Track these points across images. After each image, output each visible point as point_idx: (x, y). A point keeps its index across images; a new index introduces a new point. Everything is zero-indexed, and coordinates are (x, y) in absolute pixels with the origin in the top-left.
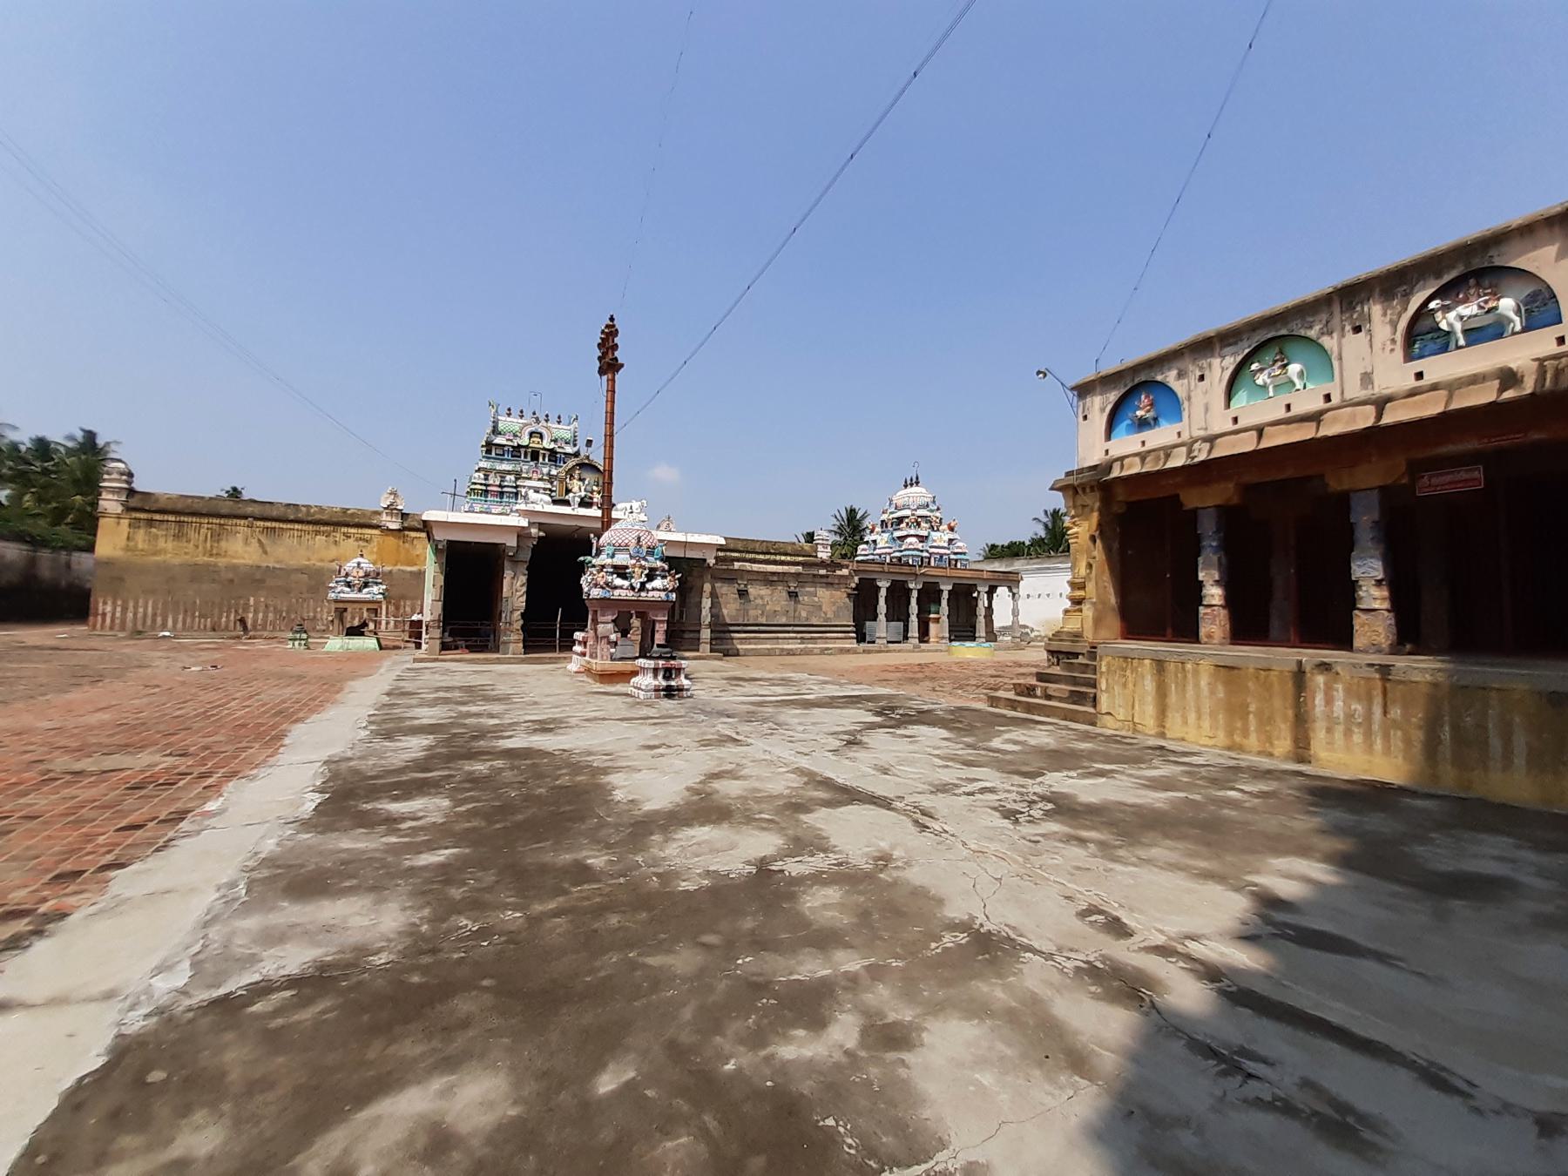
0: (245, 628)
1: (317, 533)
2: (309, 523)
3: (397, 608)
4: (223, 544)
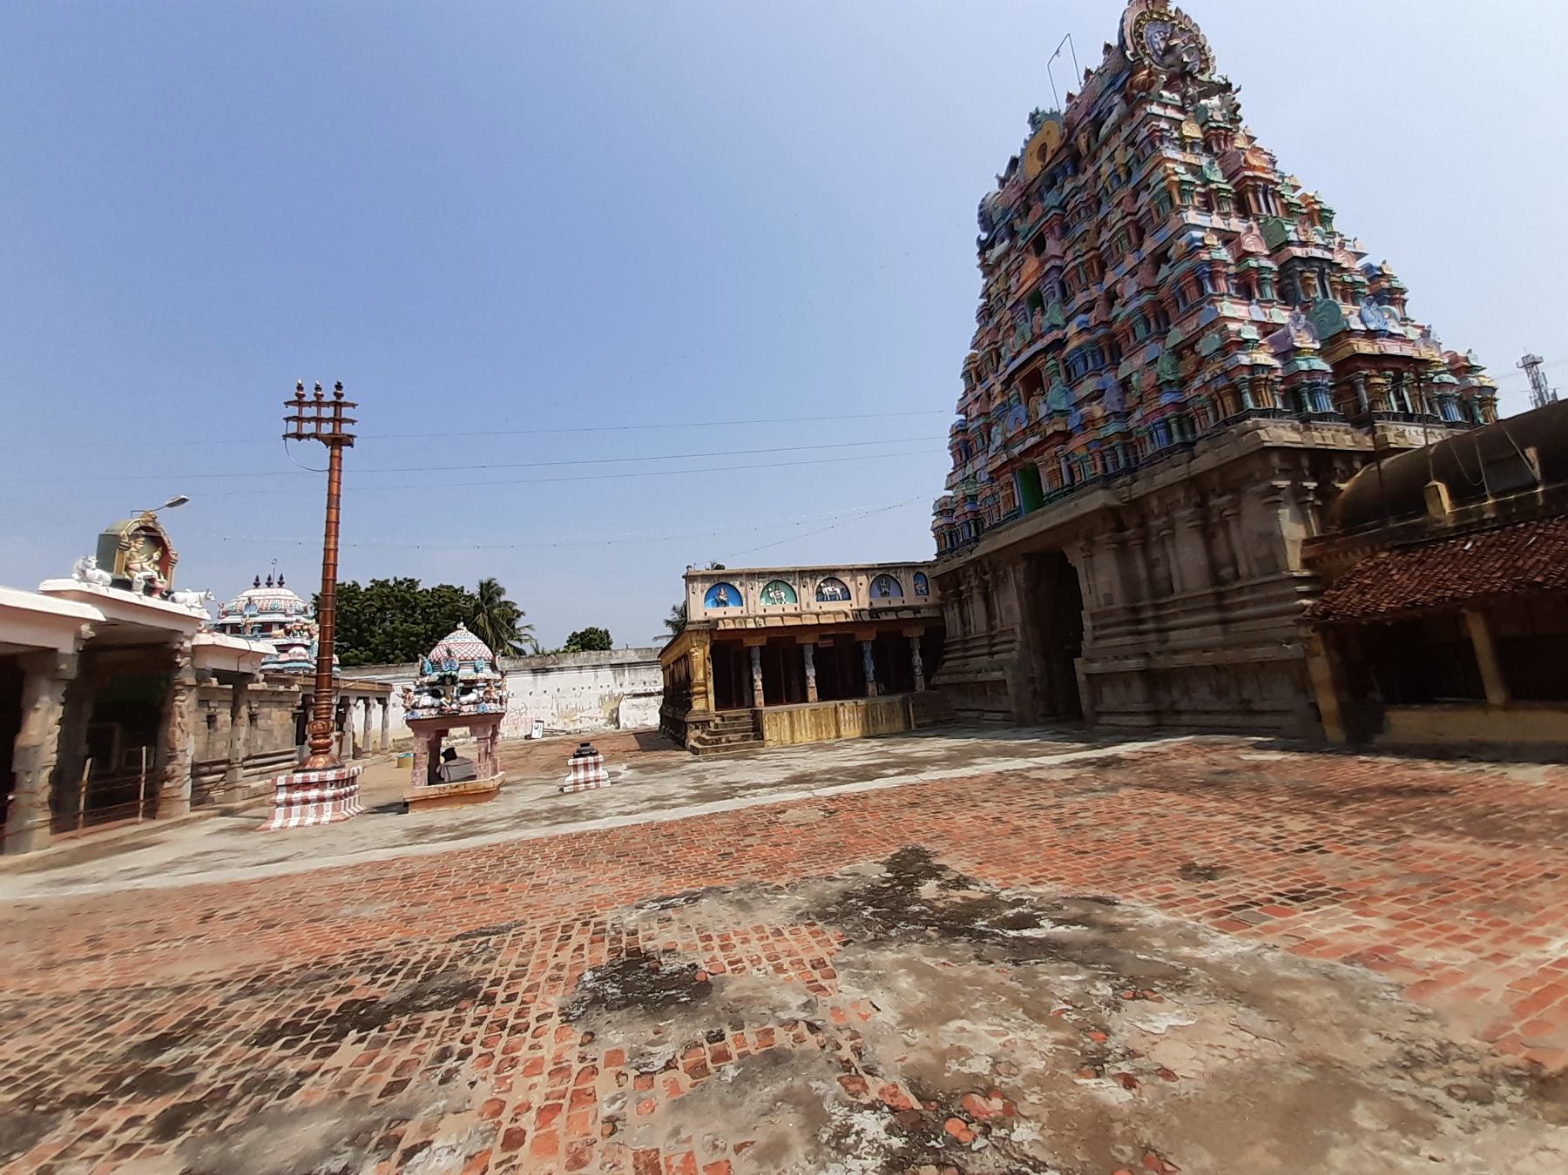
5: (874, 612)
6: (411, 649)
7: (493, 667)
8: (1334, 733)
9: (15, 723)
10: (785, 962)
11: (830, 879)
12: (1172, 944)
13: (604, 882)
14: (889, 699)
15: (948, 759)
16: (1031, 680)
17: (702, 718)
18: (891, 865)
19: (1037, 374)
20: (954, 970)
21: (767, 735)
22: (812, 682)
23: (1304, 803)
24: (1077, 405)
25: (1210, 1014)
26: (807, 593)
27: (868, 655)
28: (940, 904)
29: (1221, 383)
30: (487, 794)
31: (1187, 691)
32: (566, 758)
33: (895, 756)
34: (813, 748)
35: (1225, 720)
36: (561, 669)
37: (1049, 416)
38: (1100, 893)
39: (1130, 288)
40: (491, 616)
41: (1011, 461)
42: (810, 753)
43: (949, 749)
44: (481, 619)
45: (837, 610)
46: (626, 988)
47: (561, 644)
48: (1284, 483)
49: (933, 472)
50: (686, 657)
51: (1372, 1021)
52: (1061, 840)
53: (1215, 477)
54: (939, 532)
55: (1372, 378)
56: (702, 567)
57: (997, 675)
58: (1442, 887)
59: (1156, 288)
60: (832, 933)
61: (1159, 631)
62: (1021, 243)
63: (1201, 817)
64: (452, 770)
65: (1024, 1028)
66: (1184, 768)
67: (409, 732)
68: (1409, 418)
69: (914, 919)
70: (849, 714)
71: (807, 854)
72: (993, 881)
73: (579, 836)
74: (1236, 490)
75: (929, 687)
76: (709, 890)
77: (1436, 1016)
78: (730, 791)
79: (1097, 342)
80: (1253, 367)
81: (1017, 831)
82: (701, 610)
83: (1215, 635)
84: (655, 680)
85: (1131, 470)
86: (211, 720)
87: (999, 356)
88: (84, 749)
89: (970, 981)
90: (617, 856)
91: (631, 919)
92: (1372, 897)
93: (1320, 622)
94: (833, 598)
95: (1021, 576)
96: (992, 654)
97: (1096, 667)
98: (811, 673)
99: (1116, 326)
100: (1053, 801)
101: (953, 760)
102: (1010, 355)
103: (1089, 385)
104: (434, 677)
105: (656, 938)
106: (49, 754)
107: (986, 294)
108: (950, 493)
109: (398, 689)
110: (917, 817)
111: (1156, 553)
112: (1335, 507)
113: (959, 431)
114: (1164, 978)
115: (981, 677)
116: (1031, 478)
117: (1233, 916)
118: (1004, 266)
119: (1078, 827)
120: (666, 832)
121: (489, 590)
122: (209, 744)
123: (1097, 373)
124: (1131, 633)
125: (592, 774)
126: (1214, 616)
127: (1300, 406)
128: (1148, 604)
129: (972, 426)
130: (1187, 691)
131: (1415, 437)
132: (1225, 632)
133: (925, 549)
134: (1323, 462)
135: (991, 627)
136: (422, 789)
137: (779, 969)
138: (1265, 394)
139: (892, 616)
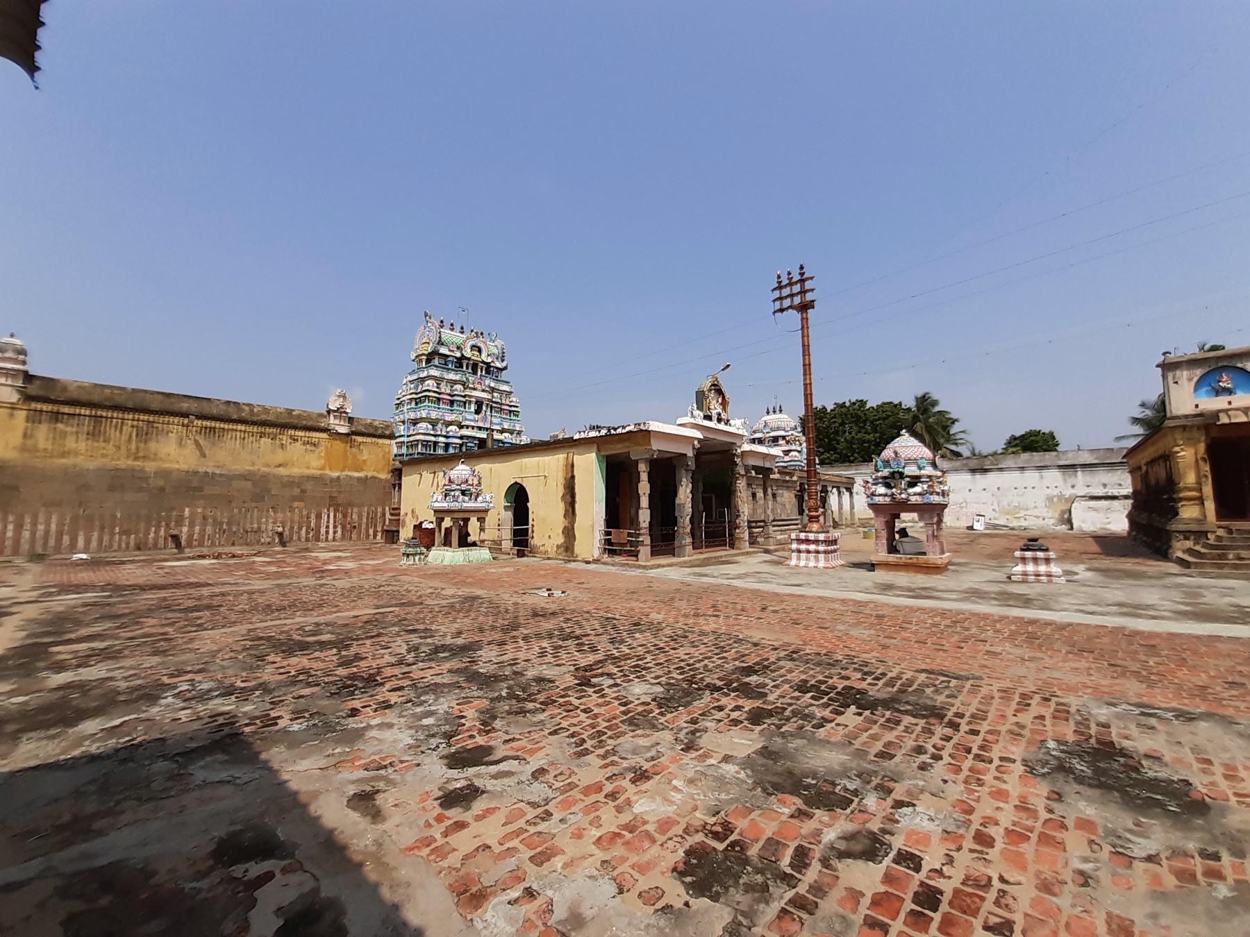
0: (178, 544)
1: (262, 435)
2: (254, 423)
3: (345, 516)
6: (866, 452)
7: (934, 465)
9: (675, 494)
13: (1064, 670)
17: (1194, 527)
36: (1001, 469)
40: (930, 423)
47: (999, 446)
50: (1167, 458)
64: (905, 545)
67: (871, 514)
73: (1033, 622)
88: (701, 507)
90: (1080, 650)
91: (1102, 713)
109: (859, 481)
120: (1151, 644)
121: (925, 403)
122: (754, 510)
125: (1042, 568)
136: (883, 555)
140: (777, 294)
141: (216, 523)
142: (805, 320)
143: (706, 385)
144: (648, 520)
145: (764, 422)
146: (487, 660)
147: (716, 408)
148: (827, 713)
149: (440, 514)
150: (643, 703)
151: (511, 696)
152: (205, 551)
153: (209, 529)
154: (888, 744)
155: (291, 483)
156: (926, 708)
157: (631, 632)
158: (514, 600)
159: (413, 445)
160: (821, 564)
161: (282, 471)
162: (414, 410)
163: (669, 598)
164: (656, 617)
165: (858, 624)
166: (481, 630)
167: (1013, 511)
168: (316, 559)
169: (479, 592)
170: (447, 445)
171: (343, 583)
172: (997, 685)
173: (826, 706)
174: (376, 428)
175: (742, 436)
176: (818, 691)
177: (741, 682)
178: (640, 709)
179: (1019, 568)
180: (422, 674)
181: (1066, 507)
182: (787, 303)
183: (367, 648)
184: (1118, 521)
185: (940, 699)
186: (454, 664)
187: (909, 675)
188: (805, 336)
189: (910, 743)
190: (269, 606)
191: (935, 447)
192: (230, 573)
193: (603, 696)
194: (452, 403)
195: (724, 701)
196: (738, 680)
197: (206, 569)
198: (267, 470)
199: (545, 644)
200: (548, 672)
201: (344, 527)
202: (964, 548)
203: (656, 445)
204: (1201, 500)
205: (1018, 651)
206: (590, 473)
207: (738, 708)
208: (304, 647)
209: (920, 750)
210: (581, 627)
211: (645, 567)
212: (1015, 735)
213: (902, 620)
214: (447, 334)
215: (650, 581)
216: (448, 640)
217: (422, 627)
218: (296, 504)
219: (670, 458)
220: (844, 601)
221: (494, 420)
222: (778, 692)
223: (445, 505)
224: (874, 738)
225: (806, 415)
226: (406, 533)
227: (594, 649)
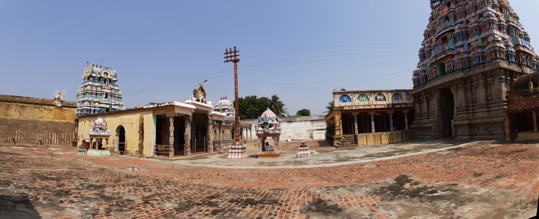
0: (14, 142)
1: (36, 108)
2: (34, 104)
3: (60, 136)
4: (9, 111)
5: (393, 105)
6: (256, 115)
7: (277, 120)
8: (508, 139)
9: (184, 131)
10: (364, 205)
11: (378, 184)
12: (470, 192)
13: (310, 182)
14: (397, 132)
15: (414, 150)
16: (439, 126)
17: (338, 137)
18: (396, 180)
19: (446, 37)
20: (414, 205)
21: (359, 143)
22: (373, 127)
23: (501, 156)
24: (457, 48)
25: (477, 206)
26: (372, 98)
27: (391, 118)
28: (410, 189)
29: (492, 49)
30: (277, 156)
31: (478, 129)
32: (298, 147)
33: (399, 149)
34: (373, 146)
35: (486, 137)
36: (296, 121)
37: (449, 50)
38: (454, 183)
39: (473, 21)
40: (275, 105)
41: (437, 61)
42: (372, 149)
43: (415, 147)
44: (273, 107)
45: (381, 104)
46: (318, 208)
47: (295, 114)
48: (504, 77)
49: (412, 63)
50: (333, 118)
51: (509, 199)
52: (445, 170)
53: (489, 73)
54: (414, 81)
55: (522, 56)
56: (338, 90)
57: (430, 125)
58: (523, 170)
59: (479, 22)
60: (378, 198)
61: (473, 113)
62: (443, 3)
63: (479, 162)
64: (268, 148)
65: (432, 216)
66: (476, 149)
67: (257, 137)
68: (528, 67)
69: (403, 193)
70: (385, 136)
71: (371, 177)
72: (425, 182)
73: (303, 169)
74: (493, 77)
75: (409, 128)
76: (341, 186)
77: (520, 195)
78: (347, 159)
79: (463, 32)
80: (500, 47)
81: (433, 169)
82: (338, 103)
83: (486, 115)
84: (324, 125)
85: (469, 68)
86: (215, 131)
87: (435, 31)
88: (195, 136)
89: (418, 207)
90: (313, 175)
91: (318, 192)
92: (512, 175)
93: (508, 112)
94: (380, 100)
95: (438, 95)
96: (428, 118)
97: (457, 123)
98: (373, 124)
99: (468, 29)
100: (443, 160)
101: (416, 150)
102: (438, 31)
103: (460, 43)
104: (262, 122)
105: (326, 197)
106: (189, 137)
107: (432, 14)
108: (418, 69)
109: (253, 126)
110: (404, 166)
111: (474, 92)
112: (513, 85)
113: (422, 51)
114: (468, 200)
115: (425, 125)
116: (442, 67)
117: (484, 184)
118: (438, 8)
119: (449, 167)
120: (328, 170)
121: (275, 98)
122: (215, 137)
123: (462, 40)
124: (466, 113)
125: (305, 152)
126: (486, 109)
127: (508, 59)
128: (471, 106)
129: (426, 50)
130: (478, 129)
131: (529, 71)
132: (488, 114)
133: (410, 86)
134: (512, 73)
135: (429, 110)
136: (261, 152)
137: (362, 206)
138: (502, 54)
139: (399, 106)
140: (226, 55)
141: (24, 136)
142: (236, 66)
143: (198, 87)
144: (173, 141)
145: (219, 103)
146: (108, 191)
147: (201, 97)
148: (240, 208)
149: (92, 137)
150: (170, 210)
151: (117, 205)
152: (21, 144)
153: (22, 138)
154: (261, 214)
155: (44, 124)
156: (272, 201)
157: (165, 185)
158: (119, 170)
159: (82, 110)
160: (240, 157)
161: (41, 120)
162: (83, 97)
163: (181, 172)
164: (175, 179)
165: (252, 177)
166: (106, 181)
167: (298, 135)
168: (51, 150)
169: (106, 167)
170: (95, 110)
171: (59, 159)
172: (293, 190)
173: (240, 206)
174: (70, 104)
175: (211, 108)
176: (237, 201)
177: (209, 202)
178: (169, 212)
179: (299, 153)
180: (84, 193)
181: (311, 133)
182: (229, 59)
183: (66, 182)
184: (322, 136)
185: (277, 197)
186: (96, 192)
187: (268, 191)
188: (236, 71)
189: (268, 212)
190: (37, 164)
191: (277, 113)
192: (27, 152)
193: (154, 207)
194: (96, 94)
195: (202, 208)
196: (208, 201)
197: (21, 150)
198: (37, 119)
199: (131, 188)
200: (132, 198)
201: (59, 140)
202: (285, 147)
203: (177, 111)
204: (340, 130)
205: (298, 179)
206: (150, 121)
207: (207, 210)
208: (47, 178)
209: (270, 214)
210: (145, 182)
211: (171, 160)
212: (297, 203)
213: (266, 174)
214: (95, 69)
215: (174, 165)
216: (94, 183)
217: (85, 177)
218: (45, 131)
219: (182, 117)
220: (247, 170)
221: (113, 101)
222: (223, 204)
223: (93, 133)
224: (256, 213)
225: (236, 100)
226: (80, 143)
227: (150, 191)
